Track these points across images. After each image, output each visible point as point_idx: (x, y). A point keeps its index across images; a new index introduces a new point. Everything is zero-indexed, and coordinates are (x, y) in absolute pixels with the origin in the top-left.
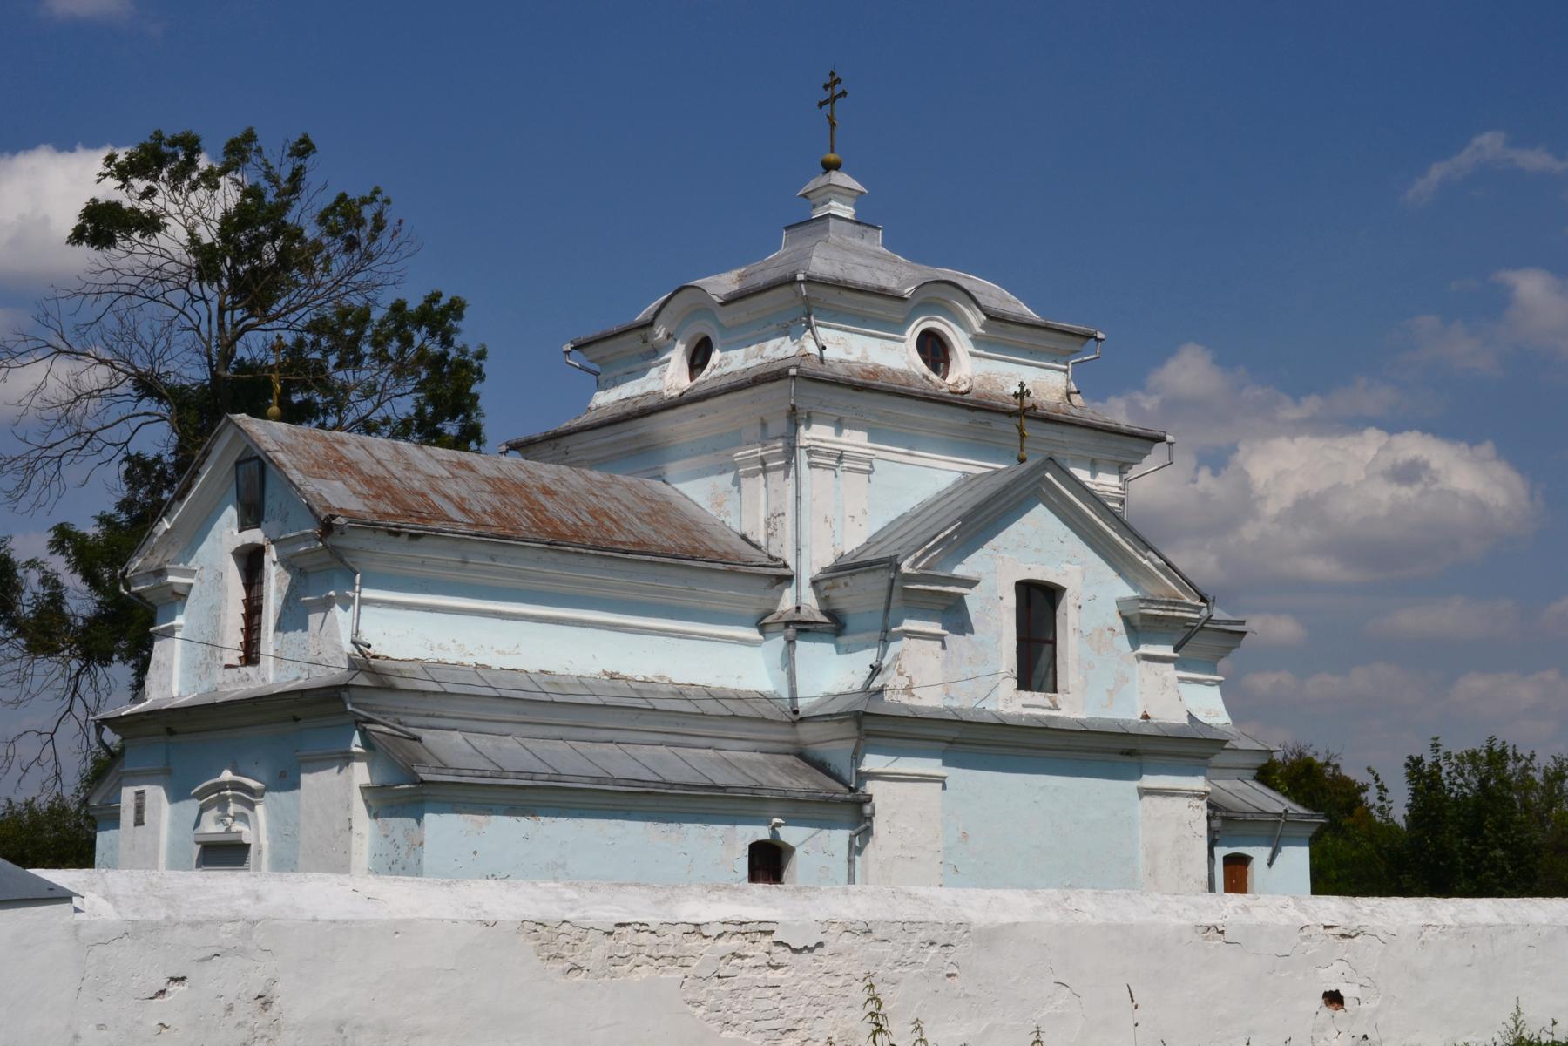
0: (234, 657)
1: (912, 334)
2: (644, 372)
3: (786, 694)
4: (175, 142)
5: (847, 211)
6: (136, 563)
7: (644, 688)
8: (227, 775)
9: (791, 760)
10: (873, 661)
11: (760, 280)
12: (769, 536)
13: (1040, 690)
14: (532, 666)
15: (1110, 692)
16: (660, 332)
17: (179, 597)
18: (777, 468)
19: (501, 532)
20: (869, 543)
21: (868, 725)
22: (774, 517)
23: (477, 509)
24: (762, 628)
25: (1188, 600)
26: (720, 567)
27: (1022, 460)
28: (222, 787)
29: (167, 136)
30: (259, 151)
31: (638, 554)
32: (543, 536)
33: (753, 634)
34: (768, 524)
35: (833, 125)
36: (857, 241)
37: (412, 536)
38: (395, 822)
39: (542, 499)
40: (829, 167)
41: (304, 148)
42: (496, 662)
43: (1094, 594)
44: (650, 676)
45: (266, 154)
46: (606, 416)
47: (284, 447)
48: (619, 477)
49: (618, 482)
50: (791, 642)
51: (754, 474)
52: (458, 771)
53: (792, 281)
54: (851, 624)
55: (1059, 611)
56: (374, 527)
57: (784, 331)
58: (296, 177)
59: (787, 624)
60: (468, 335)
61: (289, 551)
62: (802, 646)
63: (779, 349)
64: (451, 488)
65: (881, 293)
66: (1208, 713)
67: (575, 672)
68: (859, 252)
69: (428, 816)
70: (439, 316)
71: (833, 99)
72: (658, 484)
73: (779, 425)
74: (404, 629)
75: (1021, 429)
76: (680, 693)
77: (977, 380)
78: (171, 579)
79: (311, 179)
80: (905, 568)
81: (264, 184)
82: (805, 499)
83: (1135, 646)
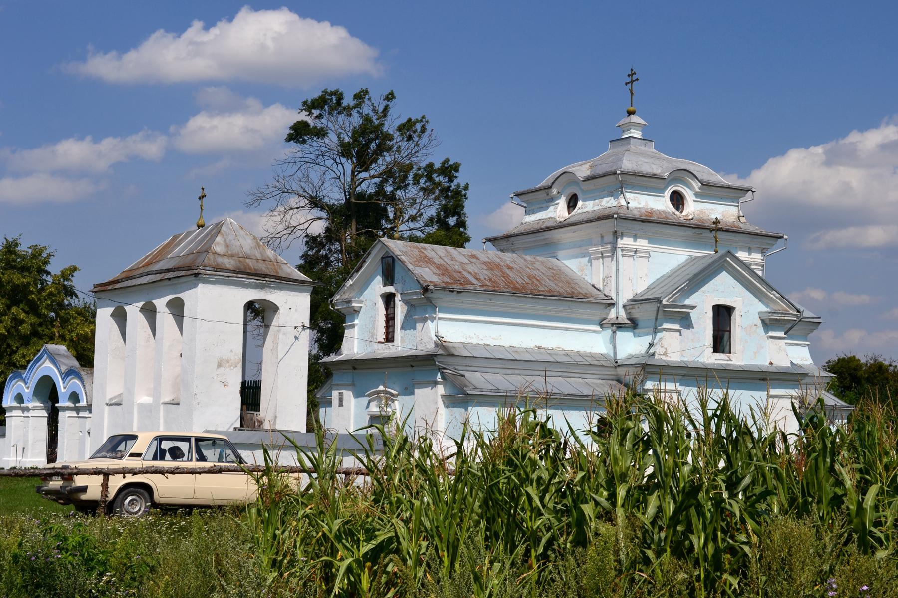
0: (381, 336)
1: (668, 193)
2: (547, 208)
3: (612, 355)
4: (332, 94)
5: (637, 134)
6: (337, 297)
7: (552, 352)
8: (381, 388)
9: (614, 383)
10: (650, 341)
11: (600, 171)
12: (604, 286)
13: (723, 352)
14: (507, 344)
15: (755, 353)
16: (555, 191)
17: (356, 312)
18: (608, 257)
19: (493, 288)
20: (648, 289)
21: (648, 369)
22: (606, 278)
23: (482, 278)
24: (601, 326)
25: (791, 312)
26: (584, 300)
27: (716, 252)
28: (378, 393)
29: (329, 91)
30: (370, 99)
31: (550, 295)
32: (510, 290)
33: (598, 328)
34: (604, 280)
35: (632, 94)
36: (643, 148)
37: (458, 292)
38: (455, 409)
39: (507, 271)
40: (630, 113)
41: (390, 97)
42: (492, 343)
43: (749, 311)
44: (554, 347)
45: (373, 101)
46: (531, 229)
47: (405, 253)
48: (538, 258)
49: (538, 261)
50: (614, 332)
51: (598, 258)
52: (481, 390)
53: (615, 173)
54: (640, 324)
55: (732, 318)
56: (444, 289)
57: (611, 195)
58: (386, 109)
59: (613, 325)
60: (461, 179)
61: (408, 297)
62: (619, 334)
63: (608, 203)
64: (471, 268)
65: (654, 177)
66: (802, 359)
67: (524, 346)
68: (643, 155)
69: (470, 408)
70: (449, 170)
71: (632, 82)
72: (554, 260)
73: (609, 238)
74: (455, 330)
75: (716, 238)
76: (567, 354)
77: (697, 212)
78: (353, 305)
79: (392, 112)
80: (664, 302)
81: (371, 114)
82: (620, 272)
83: (766, 332)
